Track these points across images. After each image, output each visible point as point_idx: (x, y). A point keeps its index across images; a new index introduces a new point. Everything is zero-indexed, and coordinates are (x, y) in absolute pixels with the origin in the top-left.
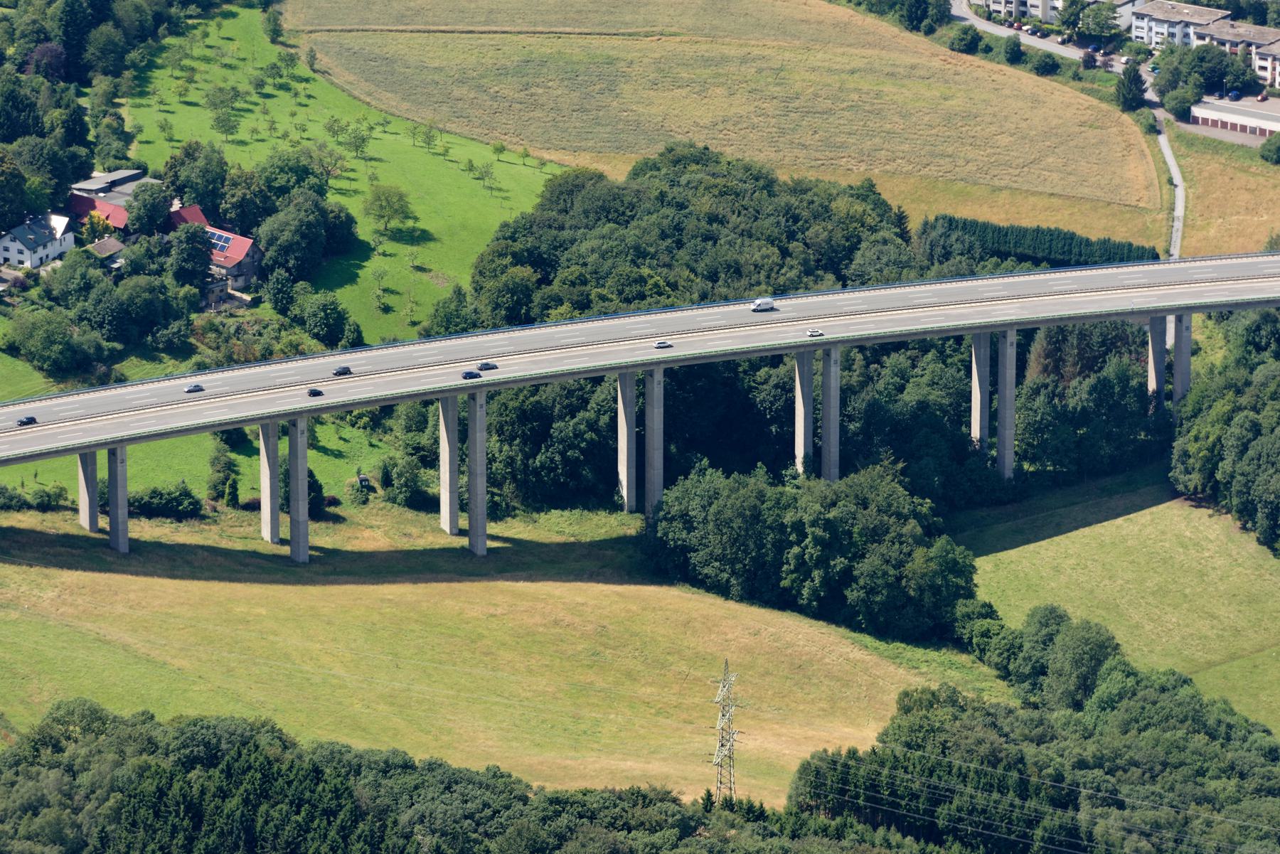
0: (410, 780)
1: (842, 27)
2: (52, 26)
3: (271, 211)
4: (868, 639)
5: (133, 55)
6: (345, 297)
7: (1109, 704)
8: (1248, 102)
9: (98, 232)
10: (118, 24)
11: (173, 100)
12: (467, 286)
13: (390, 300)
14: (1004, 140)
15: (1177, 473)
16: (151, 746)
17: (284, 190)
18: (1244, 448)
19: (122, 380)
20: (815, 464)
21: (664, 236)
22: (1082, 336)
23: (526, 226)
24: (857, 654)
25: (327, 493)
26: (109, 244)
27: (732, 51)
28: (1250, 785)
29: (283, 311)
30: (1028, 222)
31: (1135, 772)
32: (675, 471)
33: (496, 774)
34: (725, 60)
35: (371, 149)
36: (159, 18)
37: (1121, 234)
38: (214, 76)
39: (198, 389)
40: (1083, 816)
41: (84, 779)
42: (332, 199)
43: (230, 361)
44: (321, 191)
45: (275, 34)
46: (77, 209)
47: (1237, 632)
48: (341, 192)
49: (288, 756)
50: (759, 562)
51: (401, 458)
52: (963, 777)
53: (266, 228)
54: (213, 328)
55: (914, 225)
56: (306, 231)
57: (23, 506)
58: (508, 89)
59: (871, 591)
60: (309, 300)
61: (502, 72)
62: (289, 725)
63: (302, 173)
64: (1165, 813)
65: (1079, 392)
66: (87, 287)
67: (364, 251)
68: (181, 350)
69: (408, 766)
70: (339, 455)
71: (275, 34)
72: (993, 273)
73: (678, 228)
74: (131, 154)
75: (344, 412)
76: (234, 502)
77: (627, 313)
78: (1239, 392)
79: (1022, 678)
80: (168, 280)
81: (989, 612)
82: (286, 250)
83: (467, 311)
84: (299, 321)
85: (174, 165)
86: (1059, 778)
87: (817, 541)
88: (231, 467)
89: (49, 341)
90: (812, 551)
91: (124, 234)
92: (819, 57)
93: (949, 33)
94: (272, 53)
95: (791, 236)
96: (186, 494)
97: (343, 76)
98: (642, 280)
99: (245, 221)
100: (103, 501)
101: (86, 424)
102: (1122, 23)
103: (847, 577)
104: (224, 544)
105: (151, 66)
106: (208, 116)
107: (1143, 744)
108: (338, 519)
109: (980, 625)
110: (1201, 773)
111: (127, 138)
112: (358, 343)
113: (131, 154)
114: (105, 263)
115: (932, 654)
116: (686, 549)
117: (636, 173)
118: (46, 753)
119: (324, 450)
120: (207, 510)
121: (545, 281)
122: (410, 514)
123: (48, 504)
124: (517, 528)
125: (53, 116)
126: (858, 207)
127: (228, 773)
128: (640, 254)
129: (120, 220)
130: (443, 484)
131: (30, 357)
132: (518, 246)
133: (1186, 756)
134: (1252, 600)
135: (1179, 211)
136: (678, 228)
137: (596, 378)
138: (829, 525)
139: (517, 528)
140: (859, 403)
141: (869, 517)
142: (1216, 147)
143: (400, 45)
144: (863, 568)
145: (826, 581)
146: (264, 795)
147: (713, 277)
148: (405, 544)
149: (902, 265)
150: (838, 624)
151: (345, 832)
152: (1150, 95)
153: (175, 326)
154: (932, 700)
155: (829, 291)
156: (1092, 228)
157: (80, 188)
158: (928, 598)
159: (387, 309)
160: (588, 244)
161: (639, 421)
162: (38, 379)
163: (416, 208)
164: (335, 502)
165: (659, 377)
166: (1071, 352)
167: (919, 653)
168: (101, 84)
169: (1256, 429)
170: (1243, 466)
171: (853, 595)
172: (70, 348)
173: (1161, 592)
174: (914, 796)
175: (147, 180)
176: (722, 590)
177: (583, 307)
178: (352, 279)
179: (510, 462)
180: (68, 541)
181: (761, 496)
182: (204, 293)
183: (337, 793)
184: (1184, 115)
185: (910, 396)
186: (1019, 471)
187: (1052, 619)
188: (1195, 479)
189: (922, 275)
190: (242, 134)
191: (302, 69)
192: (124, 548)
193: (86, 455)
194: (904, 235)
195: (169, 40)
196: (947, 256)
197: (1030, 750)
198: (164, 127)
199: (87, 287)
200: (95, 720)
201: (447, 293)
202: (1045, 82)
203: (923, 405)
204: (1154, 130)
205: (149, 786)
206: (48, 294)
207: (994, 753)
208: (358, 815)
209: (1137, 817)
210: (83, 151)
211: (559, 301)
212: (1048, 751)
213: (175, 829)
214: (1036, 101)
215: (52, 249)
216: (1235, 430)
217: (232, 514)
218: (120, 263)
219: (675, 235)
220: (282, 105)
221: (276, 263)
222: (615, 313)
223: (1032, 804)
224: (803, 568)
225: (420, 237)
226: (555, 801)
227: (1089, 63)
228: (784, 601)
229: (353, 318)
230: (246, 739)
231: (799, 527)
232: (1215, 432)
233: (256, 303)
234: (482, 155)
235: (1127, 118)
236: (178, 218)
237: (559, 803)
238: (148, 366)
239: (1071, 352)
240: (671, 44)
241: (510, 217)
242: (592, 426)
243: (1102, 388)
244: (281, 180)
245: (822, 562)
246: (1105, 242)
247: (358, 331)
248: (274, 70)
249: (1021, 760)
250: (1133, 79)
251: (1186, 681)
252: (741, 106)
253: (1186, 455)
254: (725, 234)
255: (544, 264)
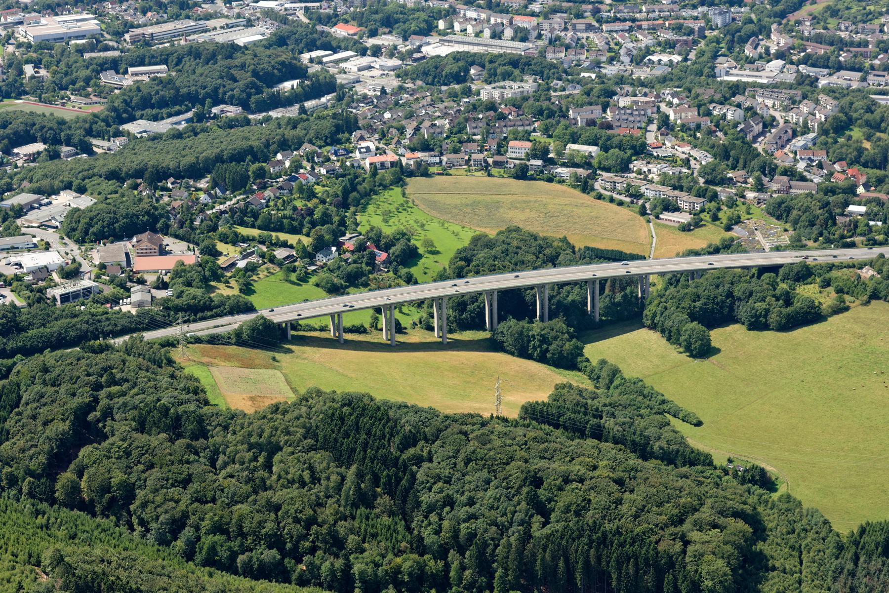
0: (406, 410)
1: (564, 192)
2: (339, 193)
3: (395, 245)
4: (552, 368)
5: (362, 201)
6: (413, 270)
7: (616, 387)
8: (676, 214)
9: (345, 252)
10: (358, 192)
11: (373, 214)
12: (447, 267)
13: (426, 271)
14: (607, 224)
15: (644, 320)
16: (333, 400)
17: (399, 239)
18: (662, 314)
19: (348, 294)
20: (542, 319)
21: (503, 252)
22: (621, 281)
23: (465, 249)
24: (549, 372)
25: (403, 326)
26: (348, 255)
27: (532, 199)
28: (654, 411)
29: (396, 274)
30: (610, 248)
31: (620, 408)
32: (501, 319)
33: (431, 409)
34: (530, 201)
35: (426, 227)
36: (371, 190)
37: (636, 251)
38: (386, 207)
39: (517, 276)
40: (603, 421)
41: (314, 410)
42: (413, 242)
43: (379, 288)
44: (409, 240)
45: (404, 195)
46: (339, 245)
47: (658, 366)
48: (416, 240)
49: (372, 403)
50: (523, 346)
51: (425, 315)
52: (568, 409)
53: (391, 251)
54: (375, 279)
55: (577, 249)
56: (403, 251)
57: (315, 330)
58: (468, 210)
59: (554, 354)
60: (403, 271)
61: (467, 205)
62: (374, 394)
63: (404, 234)
64: (627, 419)
65: (619, 297)
66: (339, 267)
67: (420, 256)
68: (366, 285)
69: (406, 406)
70: (408, 315)
71: (404, 195)
72: (596, 263)
73: (507, 250)
74: (358, 229)
75: (410, 303)
76: (376, 328)
77: (490, 275)
78: (662, 297)
79: (594, 380)
80: (364, 265)
81: (587, 360)
82: (397, 256)
83: (446, 274)
84: (400, 277)
85: (368, 232)
86: (597, 410)
87: (539, 340)
88: (377, 318)
89: (327, 283)
90: (537, 343)
91: (353, 252)
92: (557, 201)
93: (593, 194)
94: (402, 200)
95: (540, 252)
96: (362, 326)
97: (422, 207)
98: (495, 265)
99: (386, 248)
100: (337, 327)
101: (399, 296)
102: (642, 191)
103: (547, 350)
104: (372, 340)
105: (368, 204)
106: (381, 218)
107: (624, 399)
108: (406, 333)
109: (584, 364)
110: (640, 407)
111: (357, 225)
112: (416, 283)
113: (358, 229)
114: (346, 261)
115: (571, 372)
116: (503, 342)
117: (498, 234)
118: (304, 402)
119: (404, 314)
120: (368, 331)
121: (468, 266)
122: (427, 332)
123: (323, 329)
124: (457, 336)
125: (336, 219)
126: (560, 244)
127: (353, 409)
128: (495, 258)
129: (352, 248)
130: (435, 323)
131: (322, 287)
132: (461, 256)
133: (636, 403)
134: (663, 357)
135: (654, 245)
136: (507, 250)
137: (480, 293)
138: (542, 336)
139: (457, 336)
140: (554, 301)
141: (554, 333)
142: (666, 226)
143: (439, 198)
144: (551, 348)
145: (541, 351)
146: (362, 415)
147: (516, 264)
148: (424, 341)
149: (571, 261)
150: (545, 363)
151: (384, 426)
152: (648, 212)
153: (364, 278)
154: (563, 386)
155: (550, 268)
156: (627, 250)
157: (341, 239)
158: (570, 356)
159: (425, 273)
160: (481, 255)
161: (491, 305)
162: (324, 294)
163: (435, 244)
164: (405, 328)
165: (496, 293)
166: (617, 286)
167: (567, 372)
168: (352, 209)
169: (666, 308)
170: (662, 319)
171: (548, 355)
172: (333, 285)
173: (638, 354)
174: (553, 415)
175: (361, 237)
176: (512, 354)
177: (477, 273)
178: (416, 265)
179: (455, 317)
180: (327, 340)
181: (523, 327)
182: (374, 269)
183: (383, 415)
184: (657, 217)
185: (570, 298)
186: (601, 320)
187: (603, 362)
188: (649, 322)
189: (576, 264)
190: (390, 223)
191: (410, 204)
192: (342, 342)
193: (332, 315)
194: (574, 252)
195: (374, 197)
196: (585, 258)
197: (589, 401)
198: (368, 221)
199: (339, 267)
200: (319, 393)
201: (441, 269)
202: (619, 207)
203: (573, 301)
204: (649, 221)
205: (330, 412)
206: (329, 269)
207: (578, 401)
208: (389, 420)
209: (618, 421)
210: (343, 229)
211: (471, 271)
212: (596, 402)
213: (336, 425)
214: (616, 213)
215: (331, 257)
216: (660, 308)
217: (376, 332)
218: (350, 260)
219: (506, 252)
220: (403, 216)
221: (394, 260)
222: (486, 275)
223: (587, 417)
224: (535, 348)
225: (437, 253)
226: (446, 417)
227: (632, 202)
228: (529, 357)
229: (415, 276)
230: (360, 398)
231: (533, 336)
232: (655, 309)
233: (388, 271)
234: (457, 229)
235: (641, 218)
236: (368, 247)
237: (447, 417)
238: (356, 290)
239: (617, 286)
240: (515, 197)
241: (460, 247)
242: (479, 307)
243: (625, 297)
244: (398, 237)
245: (540, 346)
246: (631, 254)
247: (416, 279)
248: (402, 205)
249: (587, 404)
250: (643, 207)
251: (641, 381)
252: (533, 215)
253: (646, 315)
254: (521, 252)
255: (468, 261)
